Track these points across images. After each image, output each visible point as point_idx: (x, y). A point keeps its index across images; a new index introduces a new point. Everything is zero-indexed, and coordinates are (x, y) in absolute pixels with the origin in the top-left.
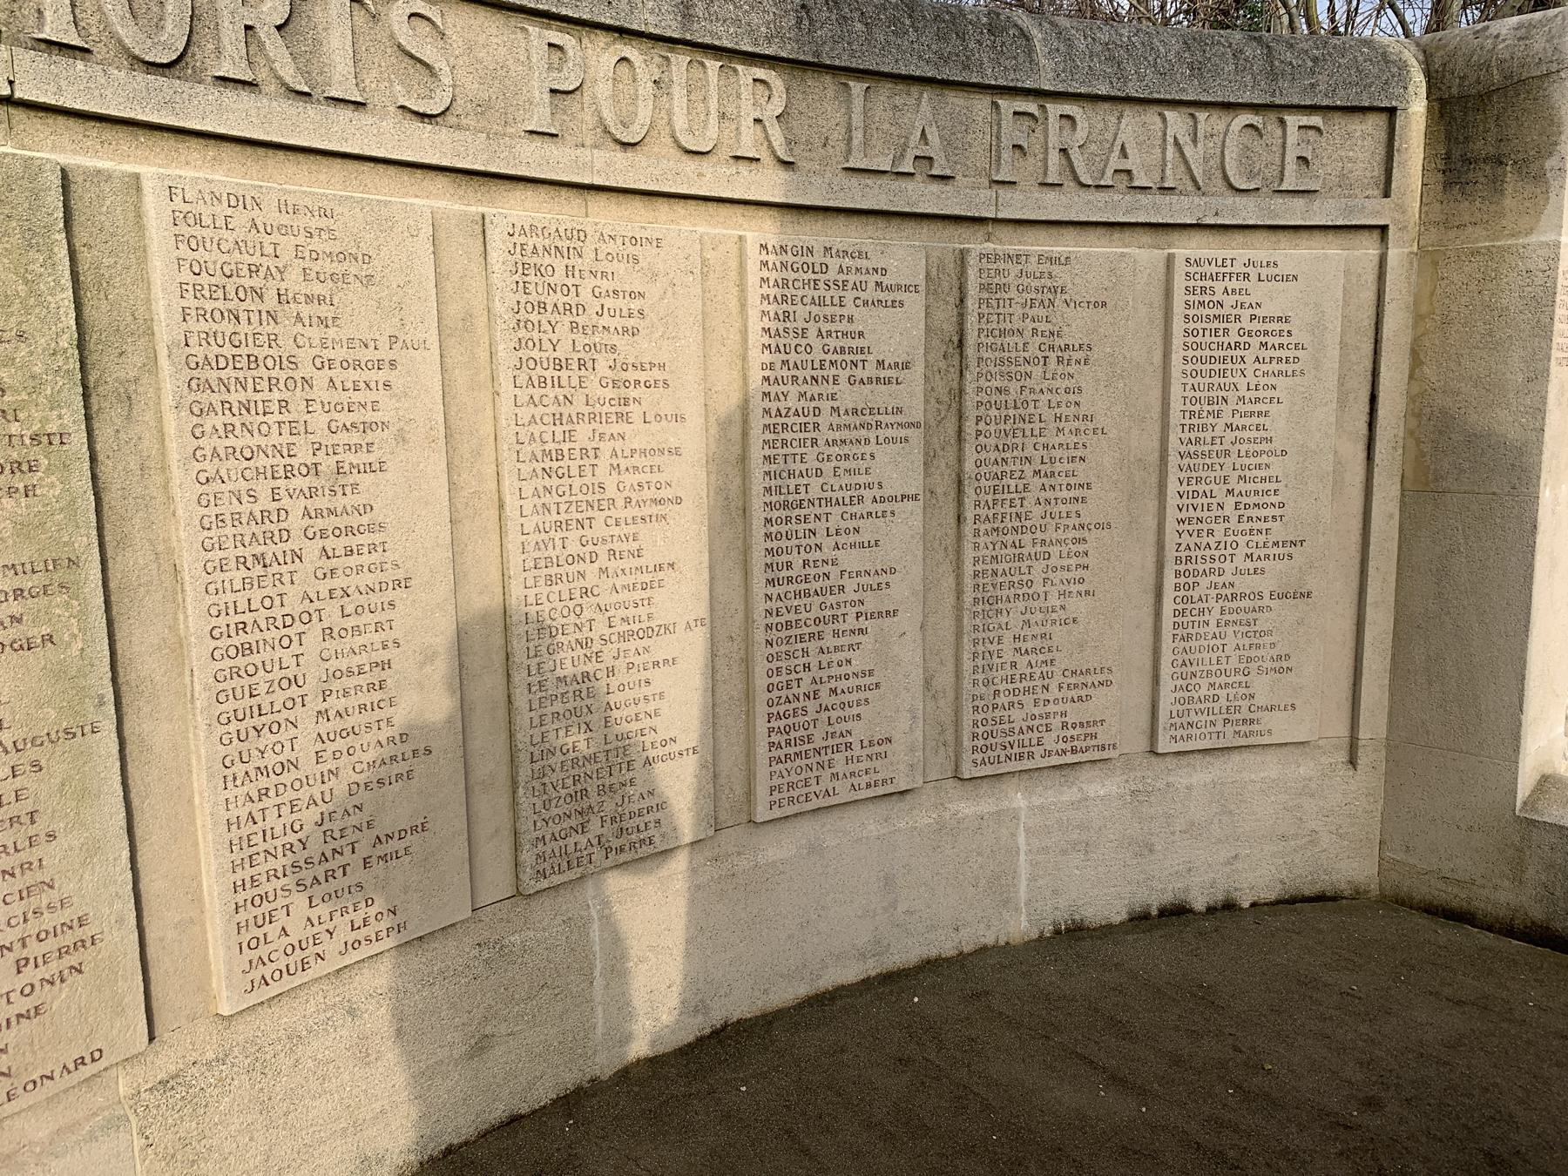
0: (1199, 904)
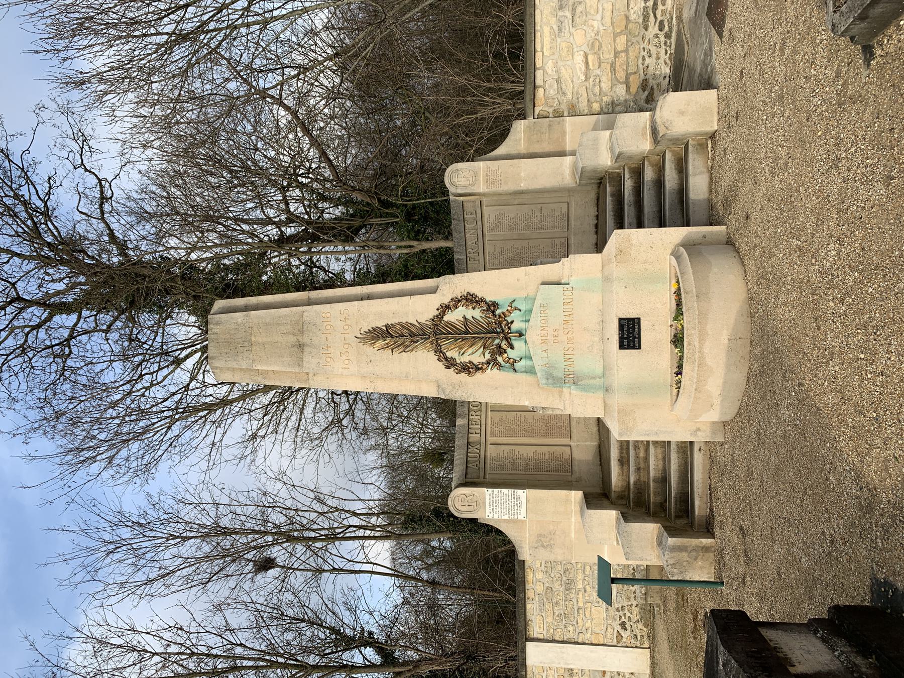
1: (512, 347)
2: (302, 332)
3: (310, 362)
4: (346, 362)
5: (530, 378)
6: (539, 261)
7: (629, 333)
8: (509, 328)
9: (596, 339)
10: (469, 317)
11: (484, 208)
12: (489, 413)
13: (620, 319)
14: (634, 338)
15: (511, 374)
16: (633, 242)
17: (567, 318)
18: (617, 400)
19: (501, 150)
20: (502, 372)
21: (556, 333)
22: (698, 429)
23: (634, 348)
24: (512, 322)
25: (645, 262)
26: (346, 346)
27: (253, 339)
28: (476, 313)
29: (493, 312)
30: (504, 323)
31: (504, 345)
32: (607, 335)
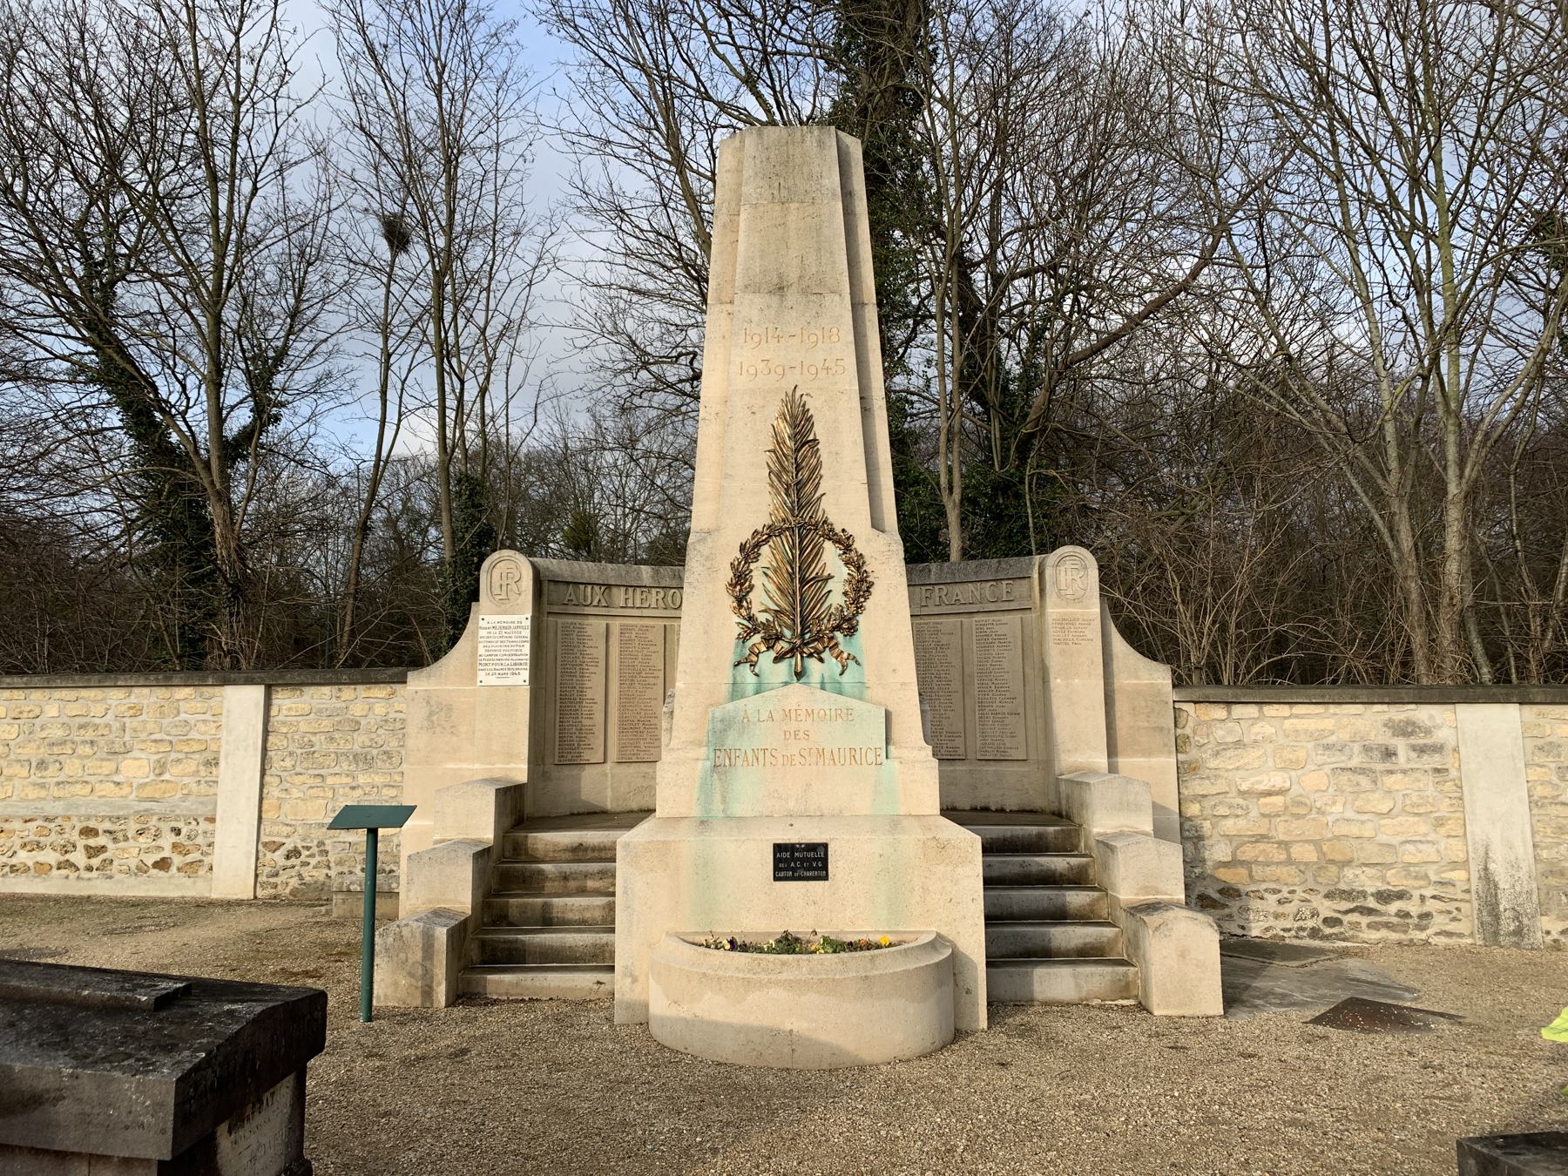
1: (777, 660)
2: (805, 292)
3: (751, 306)
4: (752, 371)
5: (725, 690)
7: (802, 860)
8: (810, 655)
9: (791, 805)
10: (830, 585)
11: (1017, 616)
12: (661, 623)
13: (825, 846)
14: (794, 870)
15: (731, 658)
16: (960, 870)
17: (828, 755)
18: (687, 842)
19: (1119, 644)
20: (734, 641)
21: (801, 735)
22: (635, 980)
23: (776, 869)
24: (821, 660)
25: (925, 889)
26: (780, 370)
27: (793, 206)
28: (836, 596)
29: (838, 628)
30: (820, 647)
31: (782, 646)
32: (798, 824)
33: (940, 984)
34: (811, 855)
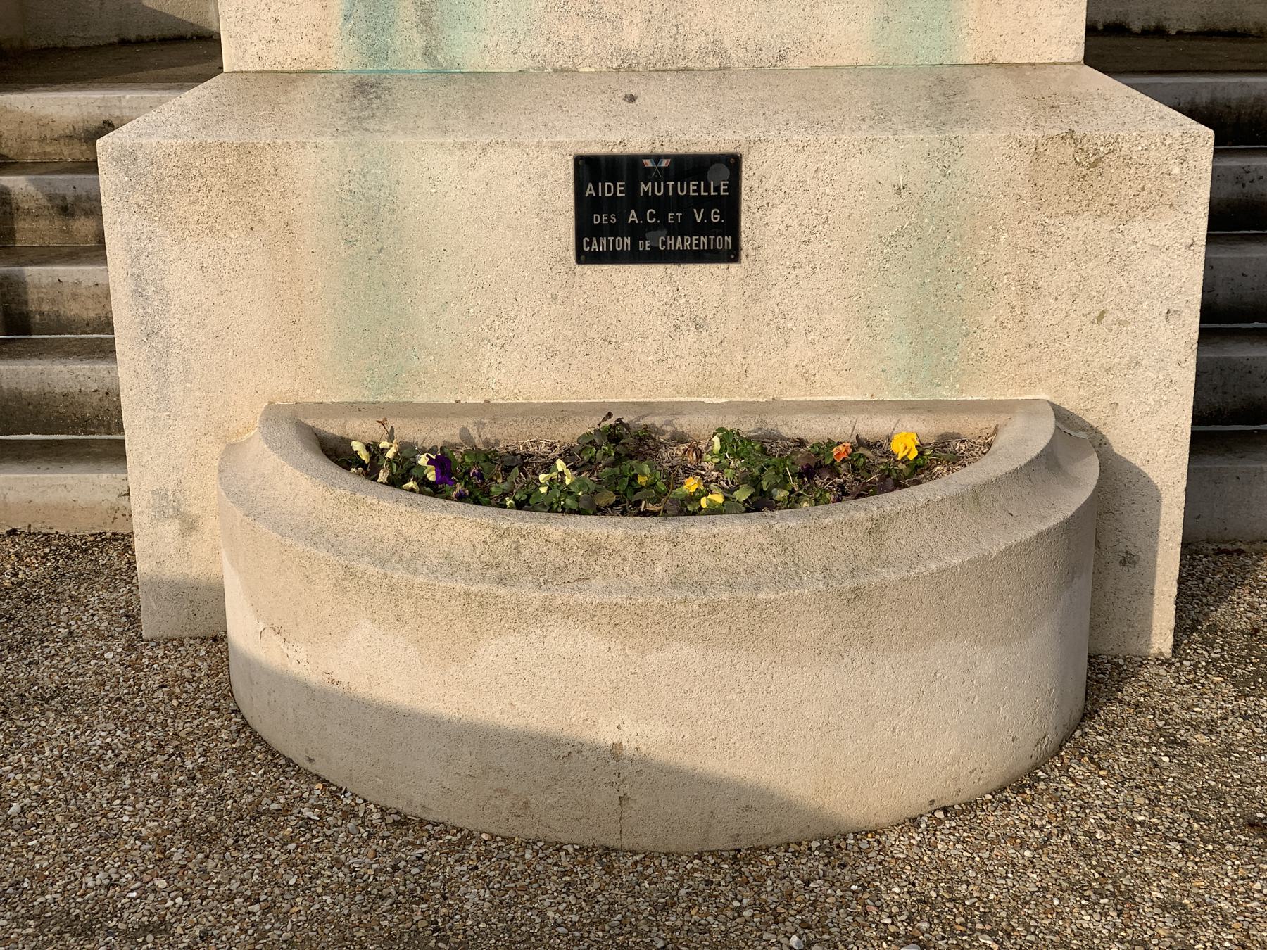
0: (1136, 27)
6: (104, 301)
7: (662, 205)
9: (632, 35)
13: (732, 163)
14: (637, 232)
16: (1138, 229)
18: (313, 159)
22: (190, 526)
23: (584, 229)
32: (652, 97)
33: (1070, 573)
34: (690, 188)
